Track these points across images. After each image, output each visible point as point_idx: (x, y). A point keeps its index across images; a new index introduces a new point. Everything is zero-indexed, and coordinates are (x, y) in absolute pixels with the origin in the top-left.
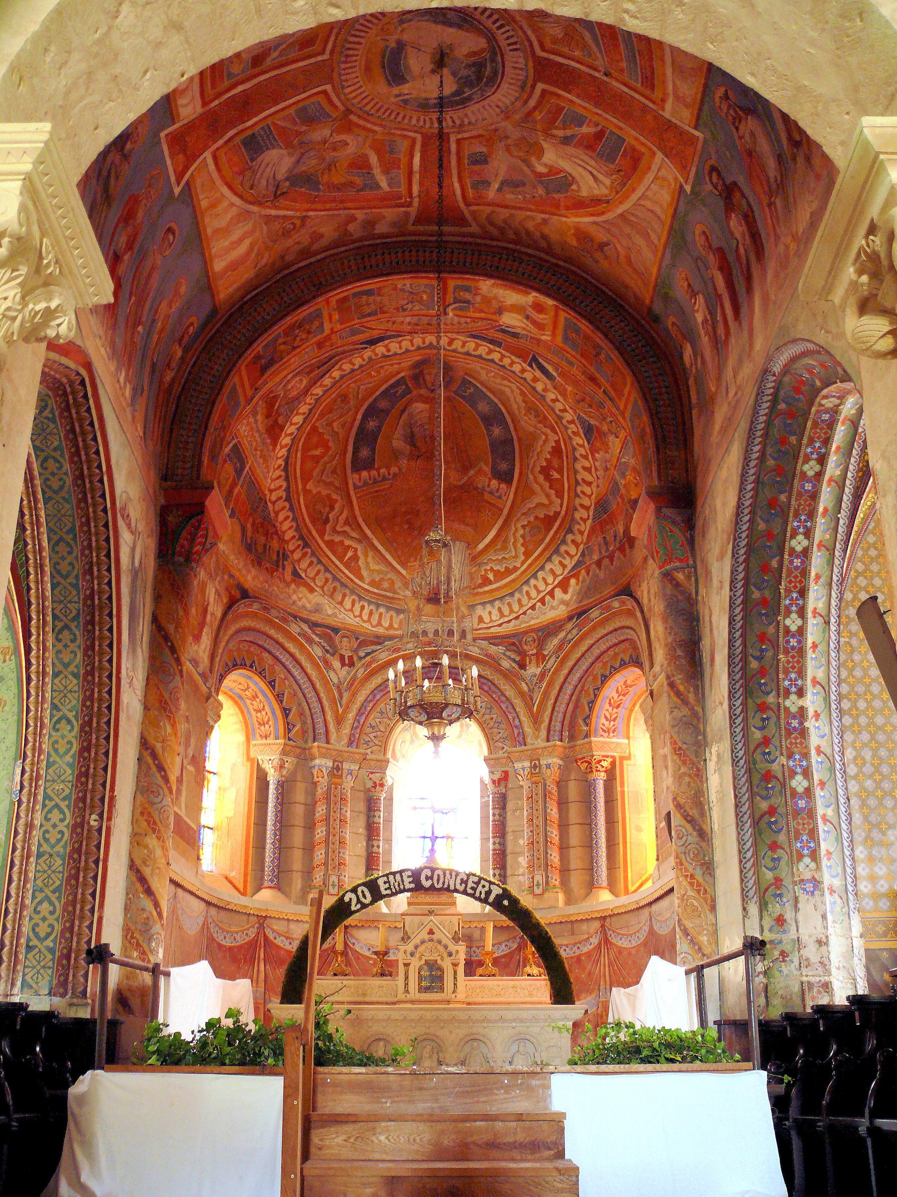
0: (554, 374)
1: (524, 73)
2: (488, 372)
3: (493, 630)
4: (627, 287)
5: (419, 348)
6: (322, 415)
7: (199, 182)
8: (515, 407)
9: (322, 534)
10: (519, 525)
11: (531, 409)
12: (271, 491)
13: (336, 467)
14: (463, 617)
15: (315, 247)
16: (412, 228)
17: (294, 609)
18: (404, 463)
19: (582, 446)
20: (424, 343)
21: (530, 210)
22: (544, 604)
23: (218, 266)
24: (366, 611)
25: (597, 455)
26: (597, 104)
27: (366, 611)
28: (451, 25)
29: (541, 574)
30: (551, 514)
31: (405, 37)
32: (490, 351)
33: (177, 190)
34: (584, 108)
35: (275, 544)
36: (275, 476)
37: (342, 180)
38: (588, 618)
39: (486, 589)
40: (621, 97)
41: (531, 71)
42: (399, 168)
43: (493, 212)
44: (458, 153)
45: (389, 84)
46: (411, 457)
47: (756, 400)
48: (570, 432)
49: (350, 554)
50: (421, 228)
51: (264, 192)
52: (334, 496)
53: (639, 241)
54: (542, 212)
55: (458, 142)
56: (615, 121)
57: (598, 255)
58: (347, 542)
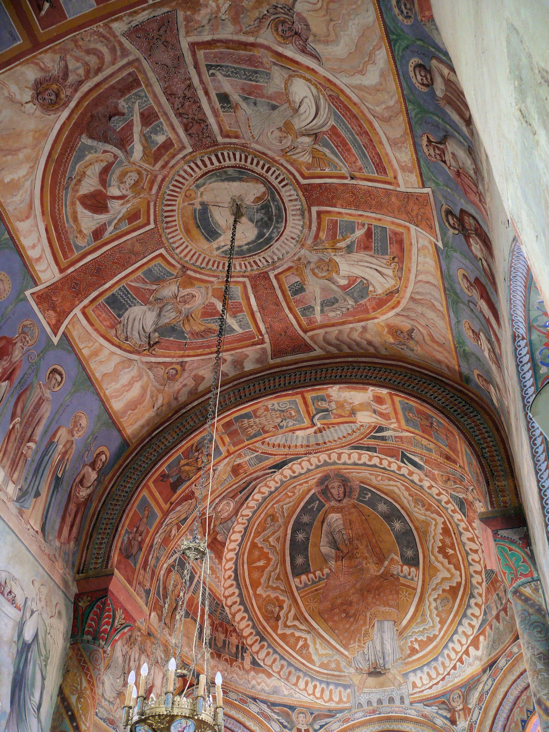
0: (422, 463)
1: (298, 203)
2: (377, 476)
3: (425, 693)
4: (439, 362)
5: (318, 467)
6: (258, 534)
7: (75, 334)
8: (405, 502)
9: (275, 629)
10: (431, 599)
11: (418, 501)
12: (226, 598)
13: (279, 575)
14: (400, 685)
15: (201, 388)
16: (271, 362)
17: (252, 693)
18: (332, 564)
19: (462, 520)
20: (319, 461)
21: (351, 322)
22: (462, 663)
23: (117, 405)
24: (318, 690)
25: (474, 524)
26: (357, 208)
27: (318, 690)
28: (233, 179)
29: (456, 637)
30: (455, 585)
31: (205, 198)
32: (371, 458)
33: (56, 340)
34: (350, 215)
35: (234, 640)
36: (227, 585)
37: (203, 328)
38: (497, 668)
39: (415, 657)
40: (369, 192)
41: (303, 198)
42: (242, 311)
43: (326, 333)
44: (280, 287)
45: (208, 240)
46: (337, 559)
47: (518, 373)
48: (449, 511)
49: (301, 643)
50: (278, 360)
51: (139, 343)
52: (281, 598)
53: (431, 314)
54: (360, 321)
55: (276, 276)
56: (373, 215)
57: (411, 344)
58: (297, 634)
